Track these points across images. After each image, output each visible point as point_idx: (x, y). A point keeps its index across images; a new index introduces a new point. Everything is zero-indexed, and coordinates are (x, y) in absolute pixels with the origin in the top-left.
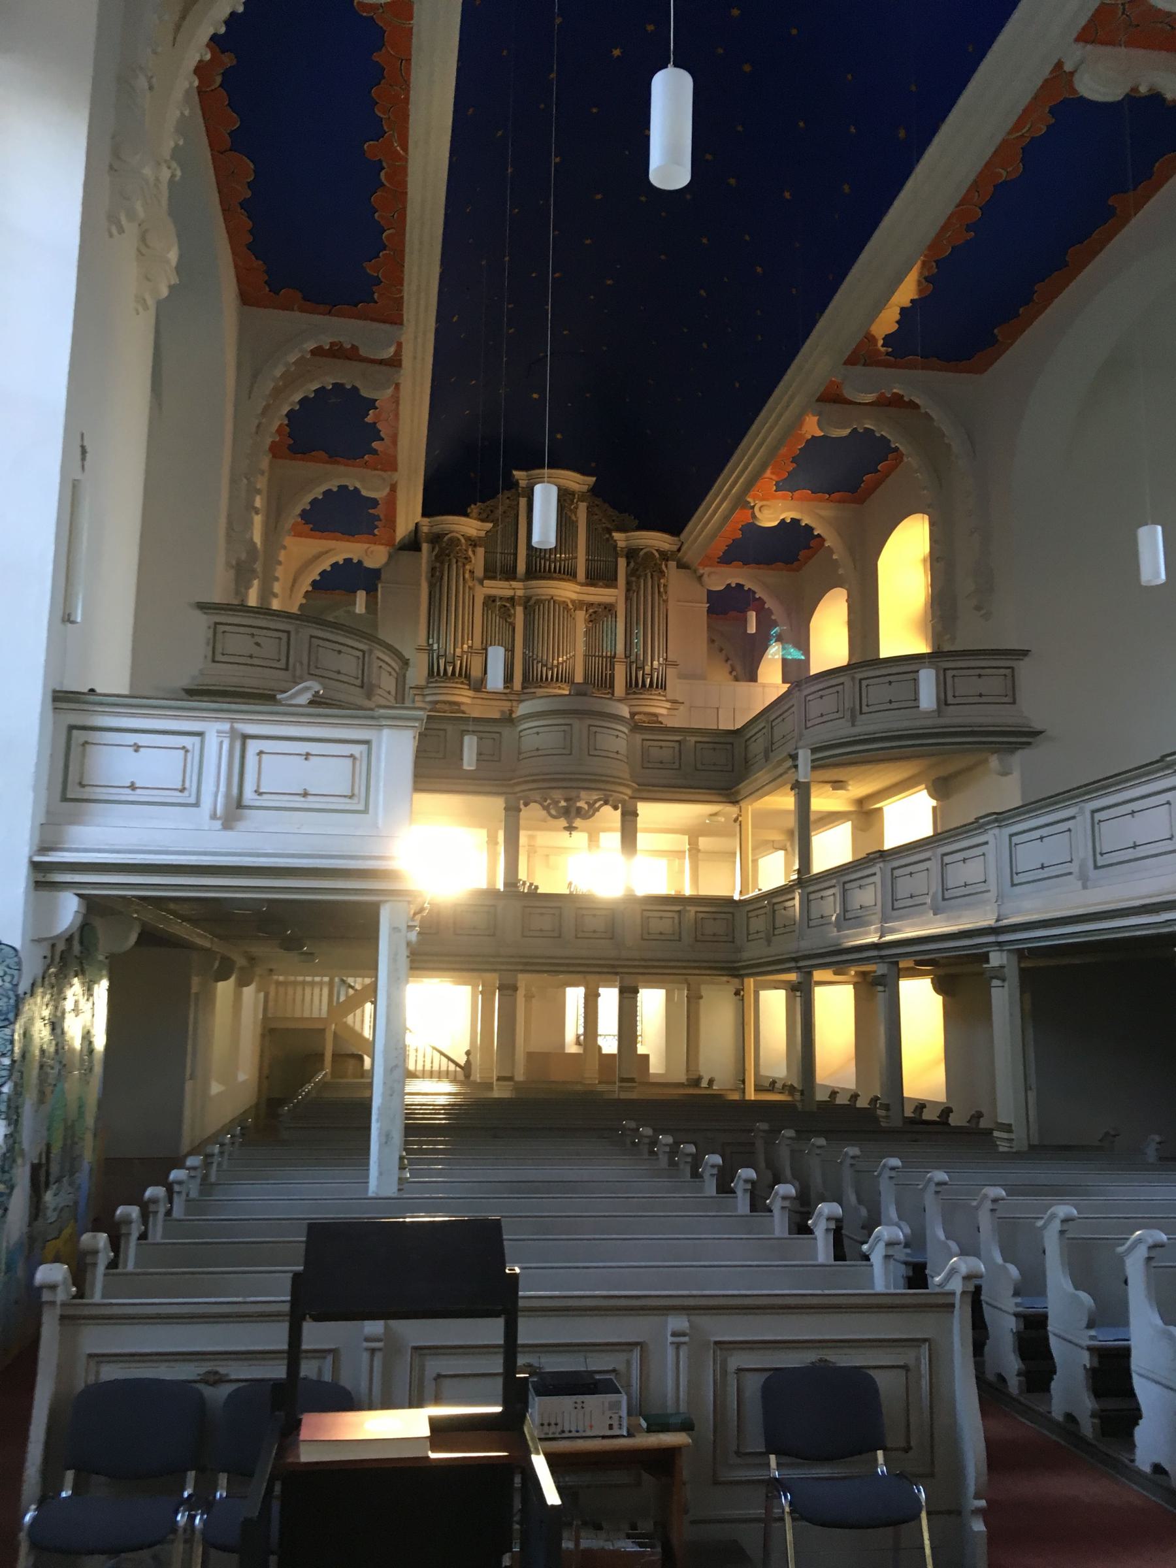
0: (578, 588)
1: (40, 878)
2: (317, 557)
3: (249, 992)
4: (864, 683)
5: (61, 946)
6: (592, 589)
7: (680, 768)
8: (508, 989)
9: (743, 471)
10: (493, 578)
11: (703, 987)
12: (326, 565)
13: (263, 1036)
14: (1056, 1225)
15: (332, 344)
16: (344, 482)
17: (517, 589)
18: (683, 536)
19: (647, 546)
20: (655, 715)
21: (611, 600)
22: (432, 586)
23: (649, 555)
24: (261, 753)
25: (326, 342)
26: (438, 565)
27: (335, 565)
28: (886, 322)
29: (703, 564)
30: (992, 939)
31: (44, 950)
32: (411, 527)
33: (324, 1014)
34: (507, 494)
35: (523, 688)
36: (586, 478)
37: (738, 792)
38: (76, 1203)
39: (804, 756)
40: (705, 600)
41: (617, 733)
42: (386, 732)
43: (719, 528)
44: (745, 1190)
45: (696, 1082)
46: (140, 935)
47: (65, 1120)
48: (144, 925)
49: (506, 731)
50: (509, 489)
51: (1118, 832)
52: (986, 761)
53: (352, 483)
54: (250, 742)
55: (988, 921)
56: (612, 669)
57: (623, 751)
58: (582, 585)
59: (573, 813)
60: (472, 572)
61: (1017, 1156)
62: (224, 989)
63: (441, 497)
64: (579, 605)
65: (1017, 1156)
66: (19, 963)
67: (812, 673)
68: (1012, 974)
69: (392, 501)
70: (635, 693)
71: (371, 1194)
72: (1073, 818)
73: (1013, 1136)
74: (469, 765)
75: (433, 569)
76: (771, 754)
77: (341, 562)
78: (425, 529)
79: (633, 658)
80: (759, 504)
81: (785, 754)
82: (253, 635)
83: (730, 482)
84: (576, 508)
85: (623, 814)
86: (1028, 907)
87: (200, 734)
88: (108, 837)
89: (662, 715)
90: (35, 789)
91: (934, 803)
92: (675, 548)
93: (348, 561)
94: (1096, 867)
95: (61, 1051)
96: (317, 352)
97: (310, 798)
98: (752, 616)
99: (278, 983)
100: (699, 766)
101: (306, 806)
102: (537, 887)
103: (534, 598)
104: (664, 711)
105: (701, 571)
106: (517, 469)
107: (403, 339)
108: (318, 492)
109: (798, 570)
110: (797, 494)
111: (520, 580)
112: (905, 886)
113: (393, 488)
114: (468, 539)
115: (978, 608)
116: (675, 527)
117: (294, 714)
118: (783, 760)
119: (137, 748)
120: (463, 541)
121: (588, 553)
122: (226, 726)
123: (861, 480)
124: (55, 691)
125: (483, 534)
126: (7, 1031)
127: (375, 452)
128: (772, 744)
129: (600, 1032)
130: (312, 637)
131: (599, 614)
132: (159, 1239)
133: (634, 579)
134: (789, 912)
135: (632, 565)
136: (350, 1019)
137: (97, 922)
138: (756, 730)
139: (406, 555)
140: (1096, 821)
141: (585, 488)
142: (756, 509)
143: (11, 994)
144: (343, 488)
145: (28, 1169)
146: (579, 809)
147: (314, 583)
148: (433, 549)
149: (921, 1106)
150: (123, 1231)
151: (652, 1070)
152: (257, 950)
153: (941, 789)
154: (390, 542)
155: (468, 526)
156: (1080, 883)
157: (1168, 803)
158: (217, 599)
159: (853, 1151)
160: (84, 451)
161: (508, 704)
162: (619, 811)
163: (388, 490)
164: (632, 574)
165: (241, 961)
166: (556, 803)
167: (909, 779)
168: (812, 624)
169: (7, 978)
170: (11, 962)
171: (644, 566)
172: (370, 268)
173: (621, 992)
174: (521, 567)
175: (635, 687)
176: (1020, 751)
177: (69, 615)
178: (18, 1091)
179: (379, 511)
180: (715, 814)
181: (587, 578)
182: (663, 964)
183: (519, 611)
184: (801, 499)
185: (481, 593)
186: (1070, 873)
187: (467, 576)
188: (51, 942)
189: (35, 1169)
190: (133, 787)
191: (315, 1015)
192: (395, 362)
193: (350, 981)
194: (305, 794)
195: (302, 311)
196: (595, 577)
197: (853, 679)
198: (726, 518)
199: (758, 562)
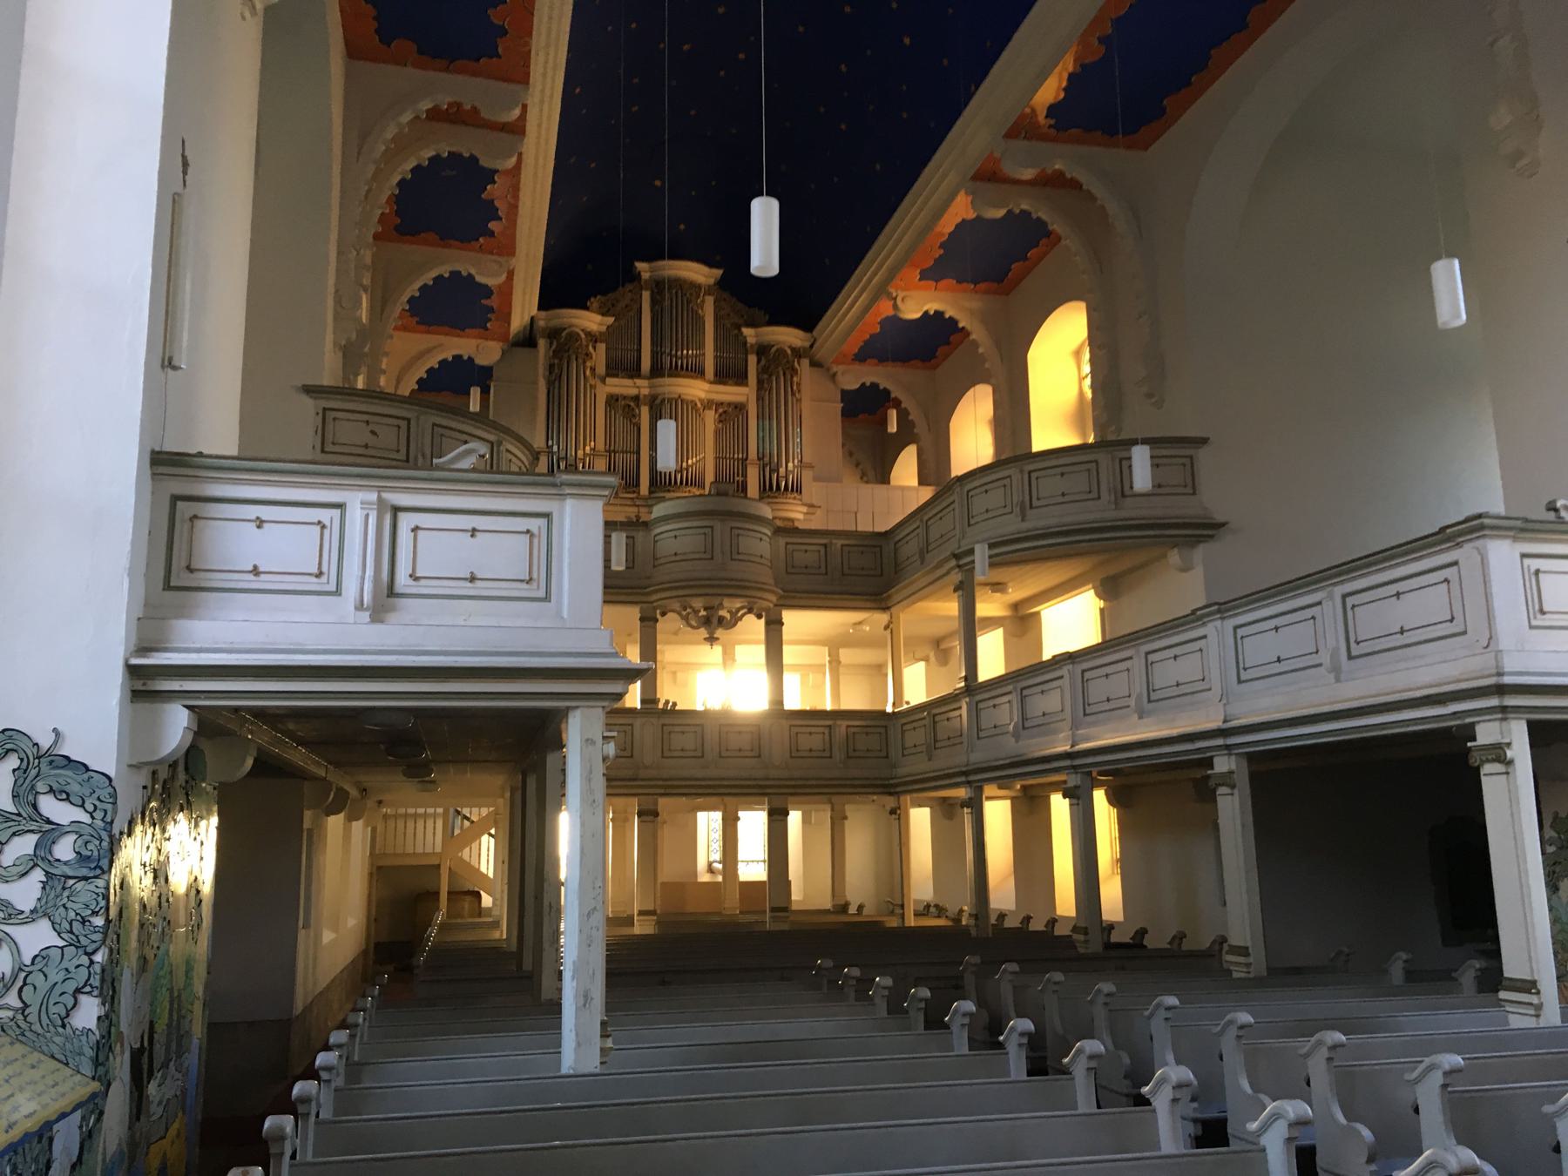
0: (706, 386)
1: (139, 686)
2: (421, 355)
3: (357, 825)
4: (1034, 475)
5: (163, 774)
6: (721, 388)
8: (649, 815)
10: (616, 376)
11: (847, 807)
12: (433, 362)
13: (371, 874)
14: (1437, 1078)
15: (450, 105)
16: (457, 267)
17: (641, 387)
18: (815, 333)
20: (792, 520)
21: (741, 399)
22: (550, 384)
23: (781, 352)
24: (415, 529)
25: (444, 101)
27: (443, 363)
28: (1050, 91)
29: (837, 362)
30: (1220, 742)
31: (143, 778)
32: (527, 319)
33: (438, 849)
34: (629, 287)
37: (889, 597)
38: (184, 1091)
39: (981, 554)
42: (569, 504)
43: (852, 328)
44: (1020, 1045)
45: (844, 908)
46: (256, 760)
47: (171, 990)
48: (260, 750)
49: (640, 536)
50: (631, 281)
51: (1377, 618)
52: (1165, 556)
53: (465, 269)
55: (1215, 723)
57: (767, 555)
59: (715, 621)
60: (593, 369)
61: (1257, 983)
62: (335, 822)
63: (560, 288)
64: (708, 404)
65: (1257, 983)
66: (114, 795)
67: (953, 475)
68: (1243, 779)
69: (507, 290)
71: (564, 1071)
72: (1319, 603)
73: (1251, 960)
75: (551, 367)
76: (928, 556)
78: (542, 323)
79: (767, 459)
80: (901, 294)
85: (768, 623)
86: (1264, 704)
87: (340, 506)
88: (220, 634)
90: (131, 573)
91: (1102, 604)
92: (807, 344)
93: (457, 358)
94: (1350, 657)
95: (165, 904)
96: (435, 115)
97: (479, 584)
98: (893, 415)
99: (385, 817)
100: (846, 571)
101: (472, 593)
102: (675, 704)
104: (801, 516)
106: (642, 260)
107: (528, 102)
108: (428, 278)
109: (935, 367)
111: (645, 378)
112: (1098, 690)
113: (511, 274)
114: (588, 334)
115: (1149, 395)
116: (807, 321)
118: (946, 560)
119: (260, 523)
121: (716, 350)
122: (373, 496)
123: (1008, 267)
124: (153, 452)
125: (604, 328)
126: (101, 883)
127: (492, 234)
129: (740, 857)
130: (434, 425)
131: (731, 415)
132: (309, 1158)
134: (956, 723)
136: (465, 854)
137: (205, 745)
139: (524, 352)
140: (1349, 606)
141: (712, 281)
143: (104, 835)
144: (455, 274)
145: (127, 1055)
146: (721, 620)
147: (420, 381)
149: (1002, 916)
150: (273, 1151)
151: (794, 897)
152: (372, 779)
153: (1110, 589)
154: (503, 337)
155: (590, 321)
156: (1332, 676)
157: (1446, 581)
158: (326, 381)
159: (1107, 987)
160: (185, 164)
162: (763, 621)
163: (504, 277)
165: (354, 792)
166: (696, 612)
167: (1081, 575)
168: (951, 424)
169: (99, 815)
170: (104, 793)
171: (775, 364)
172: (495, 16)
173: (770, 815)
174: (646, 364)
175: (769, 490)
176: (1202, 546)
177: (170, 359)
178: (114, 960)
179: (493, 302)
180: (860, 623)
182: (1047, 766)
183: (645, 411)
186: (1320, 665)
188: (152, 768)
189: (136, 1056)
190: (255, 571)
191: (429, 850)
192: (517, 129)
193: (466, 811)
194: (473, 579)
195: (415, 65)
197: (1022, 471)
198: (866, 309)
199: (894, 360)
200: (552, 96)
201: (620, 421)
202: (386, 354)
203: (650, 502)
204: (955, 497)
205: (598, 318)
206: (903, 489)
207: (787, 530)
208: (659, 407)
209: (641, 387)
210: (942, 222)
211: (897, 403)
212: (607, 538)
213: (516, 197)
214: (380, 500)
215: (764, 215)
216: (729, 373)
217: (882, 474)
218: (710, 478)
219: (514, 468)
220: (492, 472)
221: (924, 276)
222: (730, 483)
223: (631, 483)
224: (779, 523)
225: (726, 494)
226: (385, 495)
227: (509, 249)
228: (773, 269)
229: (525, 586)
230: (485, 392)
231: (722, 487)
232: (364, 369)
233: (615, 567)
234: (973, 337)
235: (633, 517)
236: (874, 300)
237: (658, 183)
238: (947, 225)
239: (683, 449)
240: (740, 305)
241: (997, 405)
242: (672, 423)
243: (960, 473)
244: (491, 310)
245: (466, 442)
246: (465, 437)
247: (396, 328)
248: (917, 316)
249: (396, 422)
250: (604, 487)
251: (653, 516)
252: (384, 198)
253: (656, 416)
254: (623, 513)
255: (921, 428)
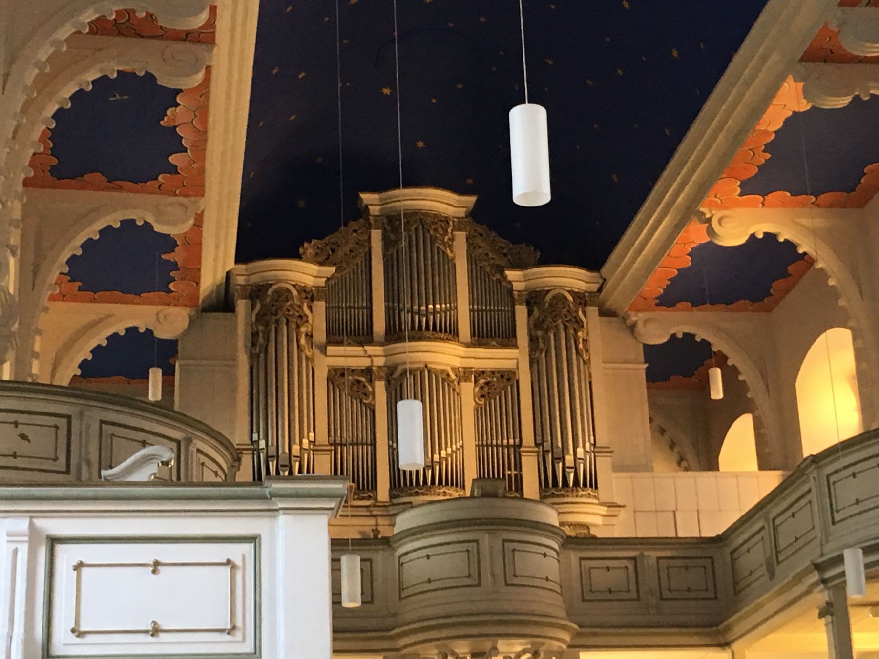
0: (462, 350)
6: (481, 351)
7: (638, 599)
9: (693, 170)
10: (340, 343)
12: (100, 338)
16: (130, 215)
17: (374, 356)
18: (605, 270)
19: (556, 287)
20: (587, 526)
21: (509, 365)
24: (79, 566)
26: (261, 328)
27: (113, 338)
32: (221, 276)
34: (353, 225)
35: (392, 496)
36: (464, 198)
37: (728, 628)
39: (854, 563)
40: (642, 358)
41: (544, 550)
42: (283, 520)
49: (379, 557)
50: (355, 219)
53: (140, 216)
54: (60, 548)
56: (519, 466)
58: (468, 345)
60: (309, 336)
64: (465, 374)
67: (806, 454)
69: (194, 242)
70: (553, 495)
74: (352, 600)
75: (255, 335)
76: (778, 569)
77: (122, 333)
78: (241, 280)
79: (547, 445)
80: (717, 214)
81: (808, 563)
82: (16, 424)
83: (673, 188)
84: (452, 239)
89: (595, 525)
92: (595, 287)
96: (99, 27)
97: (163, 637)
98: (716, 374)
103: (399, 370)
104: (598, 520)
105: (634, 319)
108: (92, 232)
110: (769, 197)
116: (593, 260)
117: (130, 497)
118: (806, 572)
120: (295, 293)
121: (472, 302)
122: (23, 524)
125: (322, 282)
127: (174, 170)
128: (778, 552)
130: (102, 422)
131: (496, 386)
133: (540, 333)
135: (536, 313)
138: (745, 536)
139: (217, 319)
141: (462, 213)
142: (714, 222)
144: (128, 224)
147: (83, 365)
148: (253, 307)
154: (191, 300)
155: (304, 272)
161: (372, 522)
163: (191, 222)
164: (536, 326)
168: (797, 384)
171: (553, 318)
174: (379, 326)
175: (553, 487)
179: (177, 256)
181: (473, 335)
183: (380, 387)
184: (783, 204)
185: (323, 365)
187: (303, 341)
192: (205, 37)
196: (482, 336)
198: (670, 238)
200: (240, 82)
201: (347, 400)
202: (39, 332)
203: (392, 509)
204: (811, 484)
205: (314, 268)
206: (737, 475)
207: (580, 541)
208: (399, 383)
209: (374, 356)
210: (765, 117)
211: (721, 360)
212: (335, 563)
213: (204, 121)
214: (33, 530)
215: (528, 130)
216: (491, 332)
217: (707, 458)
218: (471, 473)
219: (209, 477)
220: (179, 483)
221: (747, 188)
222: (500, 481)
223: (366, 485)
224: (569, 531)
225: (494, 495)
226: (39, 523)
227: (196, 187)
228: (542, 195)
229: (225, 637)
230: (168, 373)
231: (489, 486)
232: (11, 355)
233: (346, 604)
234: (819, 265)
235: (368, 530)
236: (678, 226)
237: (386, 91)
238: (773, 120)
239: (434, 435)
240: (502, 242)
241: (860, 355)
242: (417, 405)
243: (815, 452)
244: (175, 266)
245: (144, 444)
246: (141, 436)
247: (52, 298)
248: (742, 240)
249: (52, 421)
250: (330, 496)
251: (396, 530)
252: (36, 135)
253: (395, 395)
254: (354, 529)
255: (756, 390)
